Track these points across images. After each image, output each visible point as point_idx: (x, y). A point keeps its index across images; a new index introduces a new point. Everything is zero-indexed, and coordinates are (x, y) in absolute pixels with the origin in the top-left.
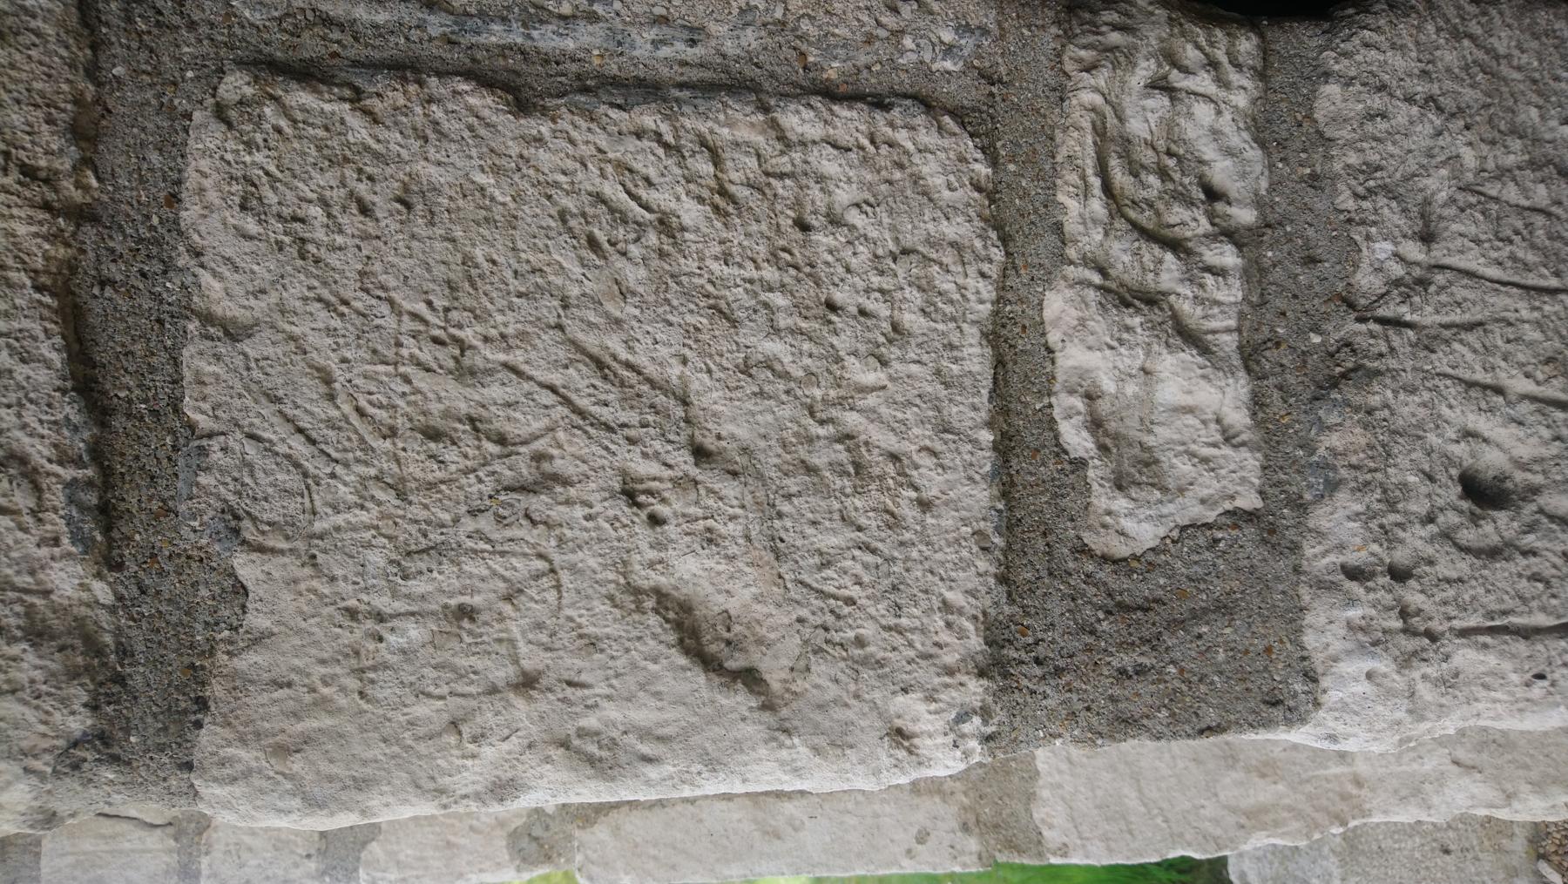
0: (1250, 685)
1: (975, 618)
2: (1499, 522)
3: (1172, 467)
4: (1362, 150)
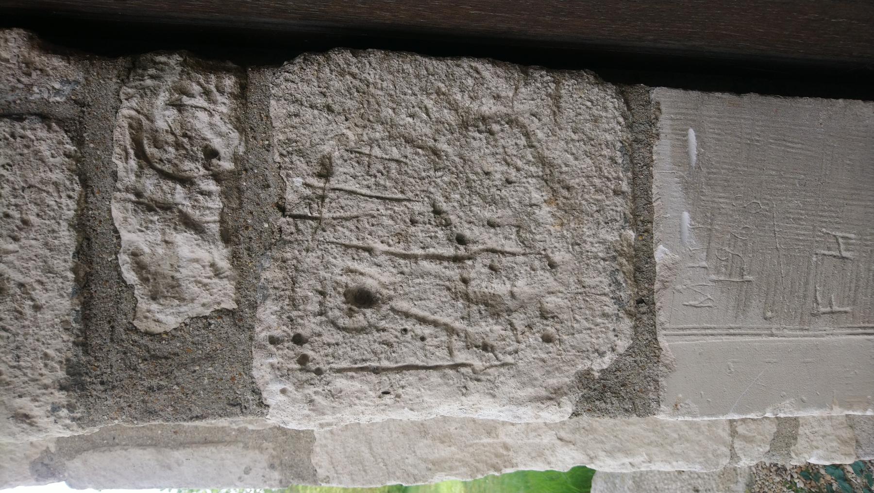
0: (221, 396)
1: (61, 362)
2: (367, 315)
3: (188, 288)
4: (285, 133)
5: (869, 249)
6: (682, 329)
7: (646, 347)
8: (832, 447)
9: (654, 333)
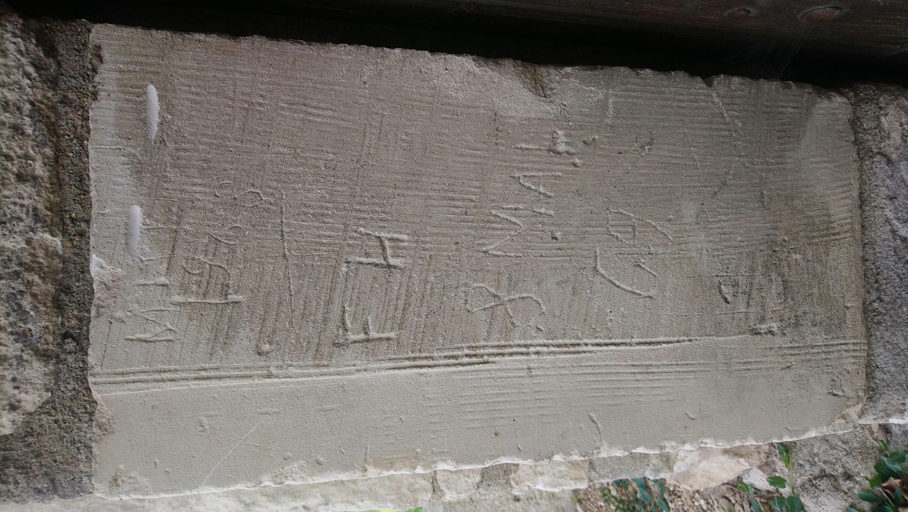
5: (428, 254)
6: (123, 374)
7: (72, 403)
8: (560, 472)
9: (84, 380)
